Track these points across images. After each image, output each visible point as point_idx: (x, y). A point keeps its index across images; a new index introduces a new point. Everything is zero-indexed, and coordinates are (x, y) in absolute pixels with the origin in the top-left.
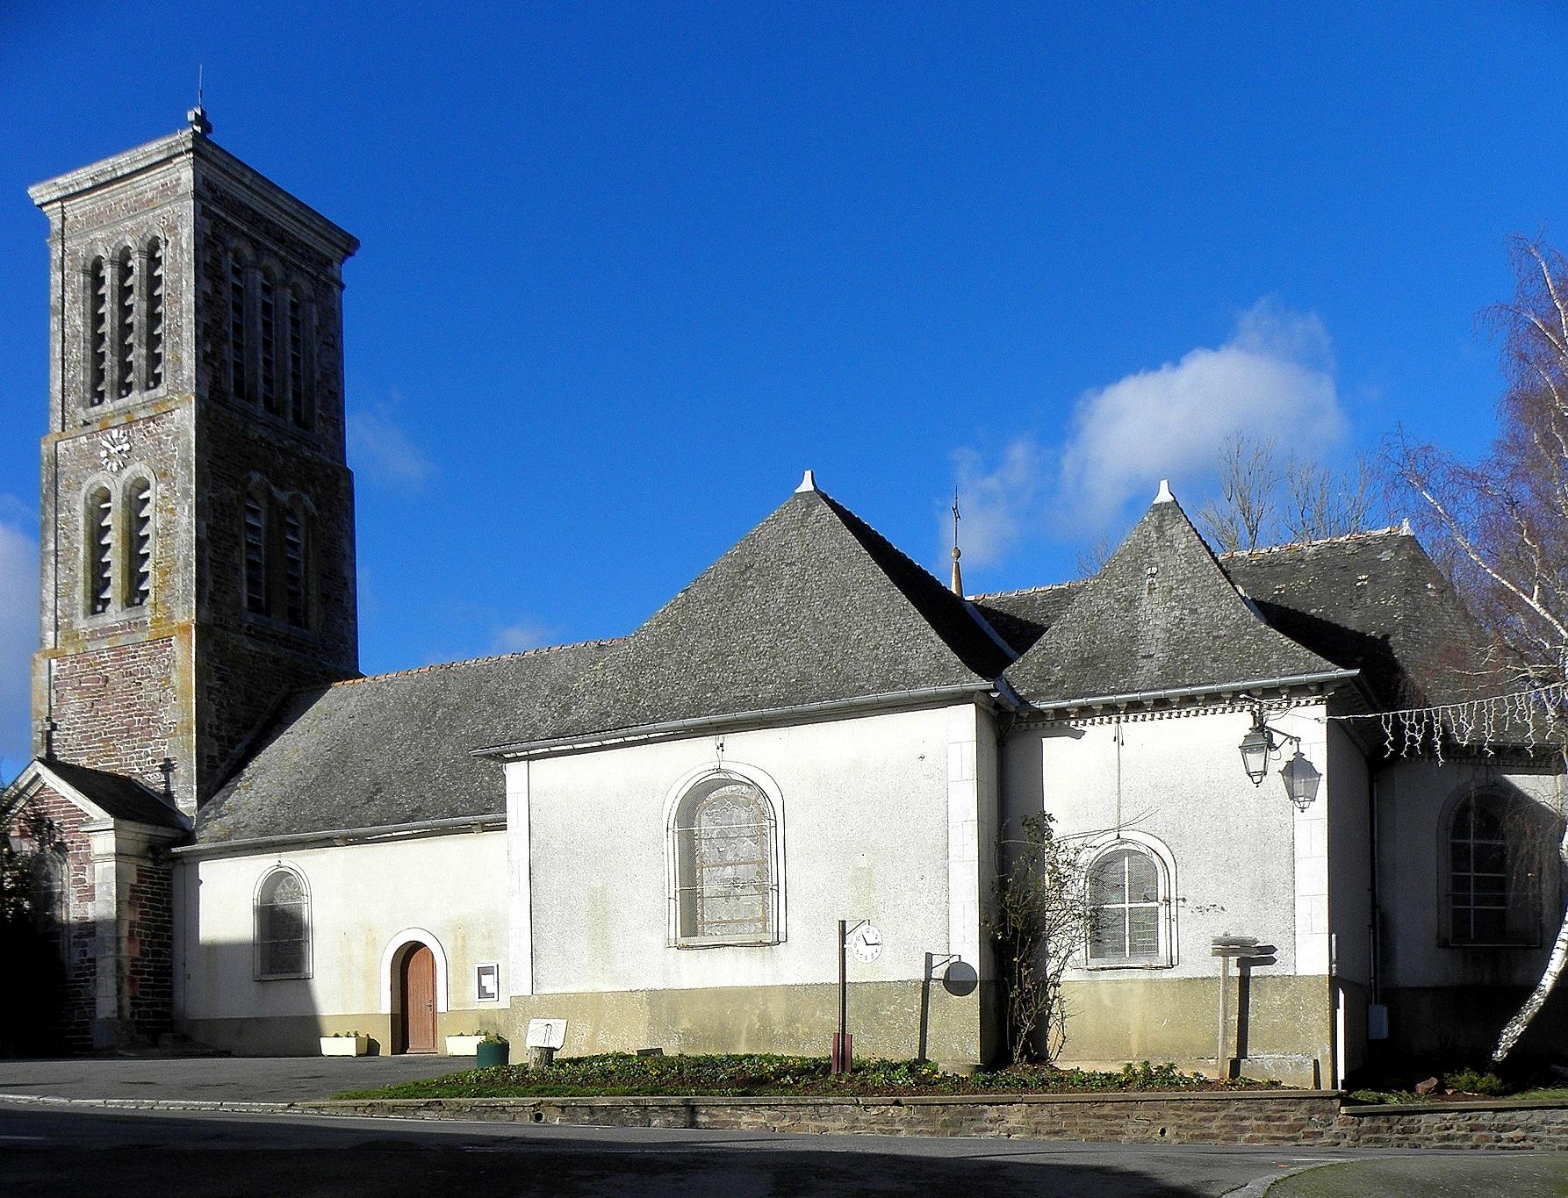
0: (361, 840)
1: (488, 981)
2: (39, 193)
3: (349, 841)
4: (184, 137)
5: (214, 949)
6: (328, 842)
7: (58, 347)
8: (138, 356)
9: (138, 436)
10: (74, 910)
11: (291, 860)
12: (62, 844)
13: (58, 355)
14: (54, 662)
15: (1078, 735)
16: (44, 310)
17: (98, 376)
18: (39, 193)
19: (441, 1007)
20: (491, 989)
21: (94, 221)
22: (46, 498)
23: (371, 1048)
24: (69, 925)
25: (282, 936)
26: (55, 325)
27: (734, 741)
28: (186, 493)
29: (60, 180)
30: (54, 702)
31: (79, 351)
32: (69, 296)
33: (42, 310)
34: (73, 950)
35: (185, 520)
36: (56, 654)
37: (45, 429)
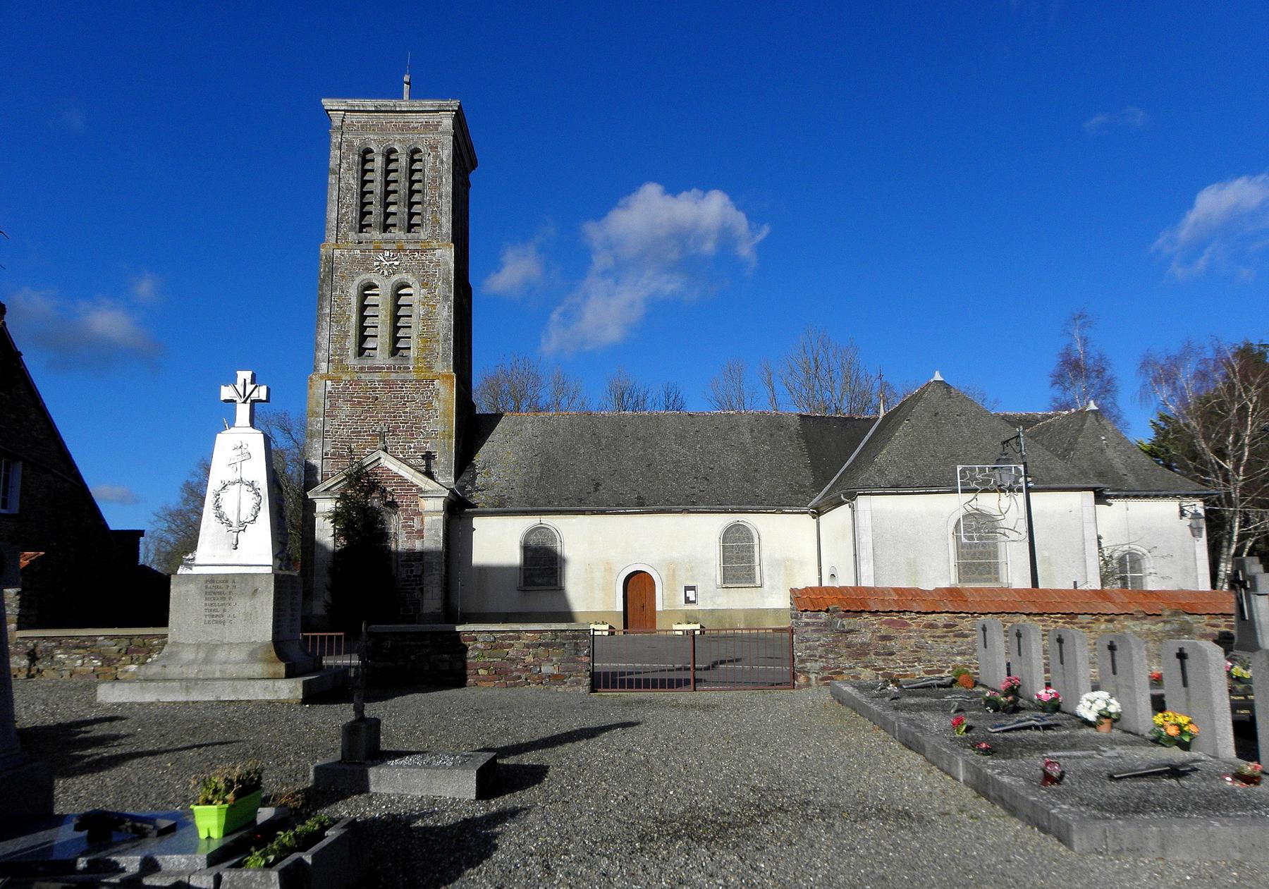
0: (603, 513)
1: (691, 594)
2: (328, 103)
3: (593, 513)
4: (454, 104)
5: (485, 570)
6: (583, 513)
7: (335, 193)
8: (376, 209)
9: (405, 258)
10: (401, 542)
11: (554, 522)
12: (393, 501)
13: (335, 197)
14: (329, 383)
15: (1110, 505)
16: (326, 171)
17: (363, 215)
18: (328, 103)
19: (659, 607)
20: (692, 599)
21: (364, 127)
22: (323, 281)
23: (612, 631)
24: (397, 553)
25: (543, 565)
26: (332, 179)
27: (981, 496)
28: (446, 298)
29: (350, 101)
30: (327, 407)
31: (352, 200)
32: (344, 165)
33: (323, 171)
34: (400, 569)
35: (445, 314)
36: (327, 377)
37: (322, 239)
